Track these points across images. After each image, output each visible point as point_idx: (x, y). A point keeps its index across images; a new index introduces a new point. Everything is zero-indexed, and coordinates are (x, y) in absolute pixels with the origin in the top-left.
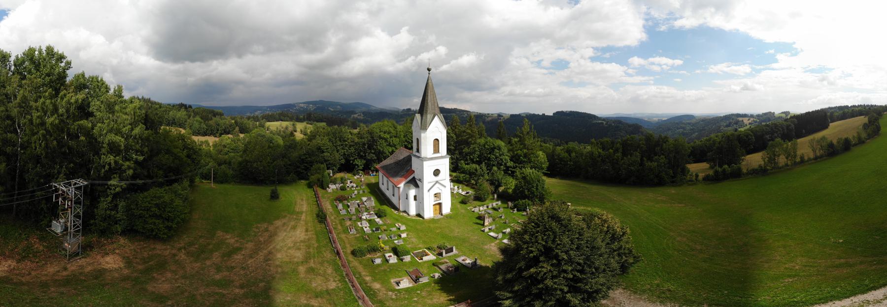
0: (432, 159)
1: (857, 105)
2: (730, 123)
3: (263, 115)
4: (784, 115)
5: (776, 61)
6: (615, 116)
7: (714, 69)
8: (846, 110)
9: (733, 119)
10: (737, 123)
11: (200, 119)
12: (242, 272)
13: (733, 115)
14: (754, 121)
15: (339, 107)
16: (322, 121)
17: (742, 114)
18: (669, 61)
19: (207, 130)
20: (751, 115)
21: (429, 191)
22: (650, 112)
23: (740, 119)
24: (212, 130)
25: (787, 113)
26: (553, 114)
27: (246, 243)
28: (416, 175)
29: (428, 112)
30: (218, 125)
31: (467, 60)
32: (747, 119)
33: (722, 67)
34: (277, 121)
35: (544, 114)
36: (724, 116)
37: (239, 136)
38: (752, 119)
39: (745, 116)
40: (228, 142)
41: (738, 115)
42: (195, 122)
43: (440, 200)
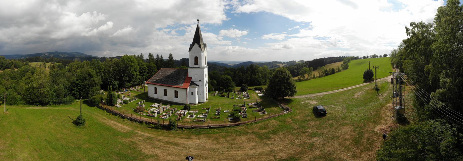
1: (339, 57)
2: (273, 66)
4: (300, 62)
5: (299, 32)
6: (212, 62)
7: (266, 37)
8: (333, 59)
9: (274, 64)
10: (276, 66)
13: (274, 62)
14: (285, 65)
15: (66, 55)
17: (279, 62)
18: (240, 32)
20: (283, 62)
22: (229, 60)
23: (278, 64)
25: (302, 61)
26: (181, 60)
30: (2, 64)
31: (127, 30)
32: (282, 64)
33: (270, 36)
34: (34, 62)
35: (176, 60)
36: (269, 62)
37: (15, 70)
38: (284, 64)
39: (280, 63)
40: (8, 73)
41: (277, 62)
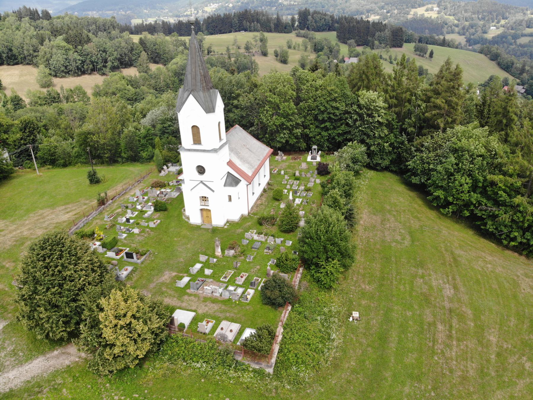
0: (189, 150)
3: (438, 342)
11: (64, 44)
16: (330, 28)
19: (83, 62)
24: (92, 62)
28: (177, 102)
42: (54, 50)
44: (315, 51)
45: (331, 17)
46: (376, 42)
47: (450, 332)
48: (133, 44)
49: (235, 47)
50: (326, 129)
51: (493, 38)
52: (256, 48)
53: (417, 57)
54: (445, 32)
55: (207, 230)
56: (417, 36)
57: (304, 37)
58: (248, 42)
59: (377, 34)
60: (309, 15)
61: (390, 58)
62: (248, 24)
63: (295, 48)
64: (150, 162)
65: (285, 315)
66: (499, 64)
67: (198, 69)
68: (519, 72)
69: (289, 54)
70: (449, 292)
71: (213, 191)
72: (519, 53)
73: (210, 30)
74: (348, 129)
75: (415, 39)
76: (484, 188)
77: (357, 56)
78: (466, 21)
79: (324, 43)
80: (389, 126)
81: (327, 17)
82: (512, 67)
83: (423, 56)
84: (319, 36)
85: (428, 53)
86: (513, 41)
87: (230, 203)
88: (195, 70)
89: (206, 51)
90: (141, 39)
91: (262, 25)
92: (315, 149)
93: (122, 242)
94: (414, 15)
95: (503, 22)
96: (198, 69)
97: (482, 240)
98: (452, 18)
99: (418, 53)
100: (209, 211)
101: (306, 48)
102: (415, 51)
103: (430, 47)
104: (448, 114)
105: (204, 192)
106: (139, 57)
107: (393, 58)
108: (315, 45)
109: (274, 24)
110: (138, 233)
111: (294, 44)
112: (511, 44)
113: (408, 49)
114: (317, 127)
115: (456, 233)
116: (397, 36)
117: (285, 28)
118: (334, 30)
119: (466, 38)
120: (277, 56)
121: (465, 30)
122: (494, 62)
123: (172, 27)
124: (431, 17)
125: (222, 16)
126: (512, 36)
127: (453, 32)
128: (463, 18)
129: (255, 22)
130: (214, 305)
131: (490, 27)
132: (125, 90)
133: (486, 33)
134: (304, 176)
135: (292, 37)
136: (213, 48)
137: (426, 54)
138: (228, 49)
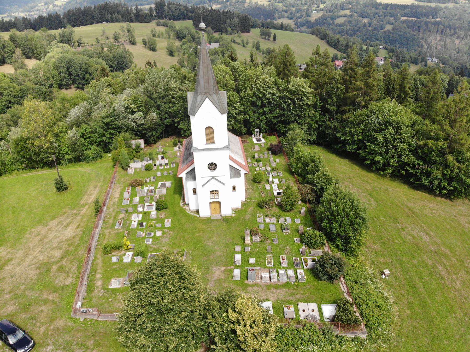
0: (203, 150)
12: (11, 280)
16: (185, 17)
21: (203, 186)
27: (16, 253)
29: (199, 92)
43: (218, 198)
44: (178, 38)
45: (184, 7)
46: (229, 29)
47: (447, 269)
48: (4, 41)
49: (104, 38)
50: (264, 113)
51: (316, 20)
52: (124, 38)
53: (263, 40)
54: (277, 17)
55: (219, 220)
56: (259, 22)
57: (164, 25)
58: (116, 32)
59: (228, 21)
60: (165, 6)
61: (243, 42)
62: (109, 15)
63: (159, 37)
64: (96, 160)
65: (343, 286)
66: (328, 43)
67: (210, 73)
68: (344, 48)
69: (157, 42)
70: (426, 238)
71: (224, 184)
72: (337, 31)
73: (72, 23)
74: (282, 112)
75: (259, 25)
76: (416, 150)
77: (217, 41)
78: (293, 7)
79: (185, 31)
80: (315, 106)
81: (181, 7)
82: (338, 44)
83: (268, 39)
84: (179, 25)
85: (272, 36)
86: (332, 22)
87: (234, 192)
88: (208, 74)
89: (76, 44)
90: (11, 36)
91: (123, 16)
92: (257, 132)
93: (152, 247)
94: (249, 3)
95: (322, 6)
96: (210, 73)
97: (416, 191)
98: (280, 5)
99: (264, 37)
100: (219, 203)
101: (169, 36)
102: (261, 35)
103: (273, 31)
104: (366, 93)
105: (214, 185)
106: (14, 53)
107: (245, 42)
108: (177, 33)
109: (134, 15)
110: (161, 235)
111: (158, 33)
112: (330, 25)
113: (255, 32)
114: (254, 112)
115: (398, 189)
116: (244, 22)
117: (145, 18)
118: (189, 19)
119: (294, 21)
120: (145, 45)
121: (293, 15)
122: (324, 41)
123: (32, 22)
124: (264, 4)
125: (83, 9)
126: (330, 18)
127: (283, 17)
128: (290, 4)
129: (116, 14)
130: (279, 290)
131: (312, 12)
132: (10, 88)
133: (309, 16)
134: (262, 157)
135: (152, 25)
136: (83, 40)
137: (270, 37)
138: (98, 40)
